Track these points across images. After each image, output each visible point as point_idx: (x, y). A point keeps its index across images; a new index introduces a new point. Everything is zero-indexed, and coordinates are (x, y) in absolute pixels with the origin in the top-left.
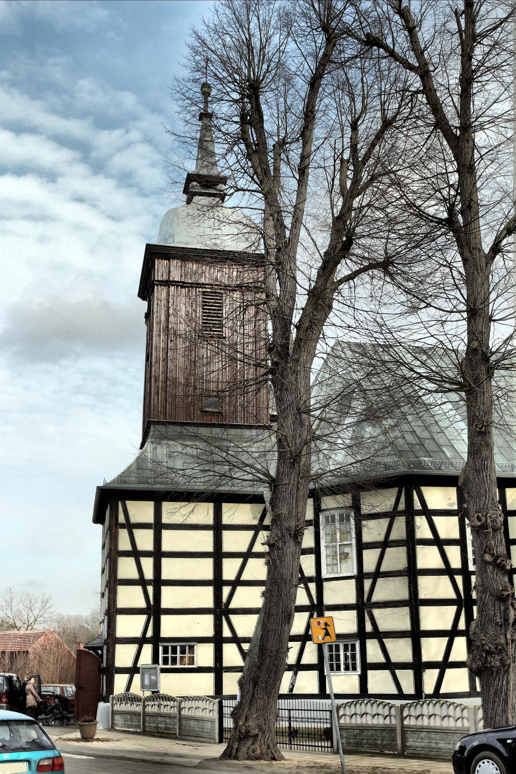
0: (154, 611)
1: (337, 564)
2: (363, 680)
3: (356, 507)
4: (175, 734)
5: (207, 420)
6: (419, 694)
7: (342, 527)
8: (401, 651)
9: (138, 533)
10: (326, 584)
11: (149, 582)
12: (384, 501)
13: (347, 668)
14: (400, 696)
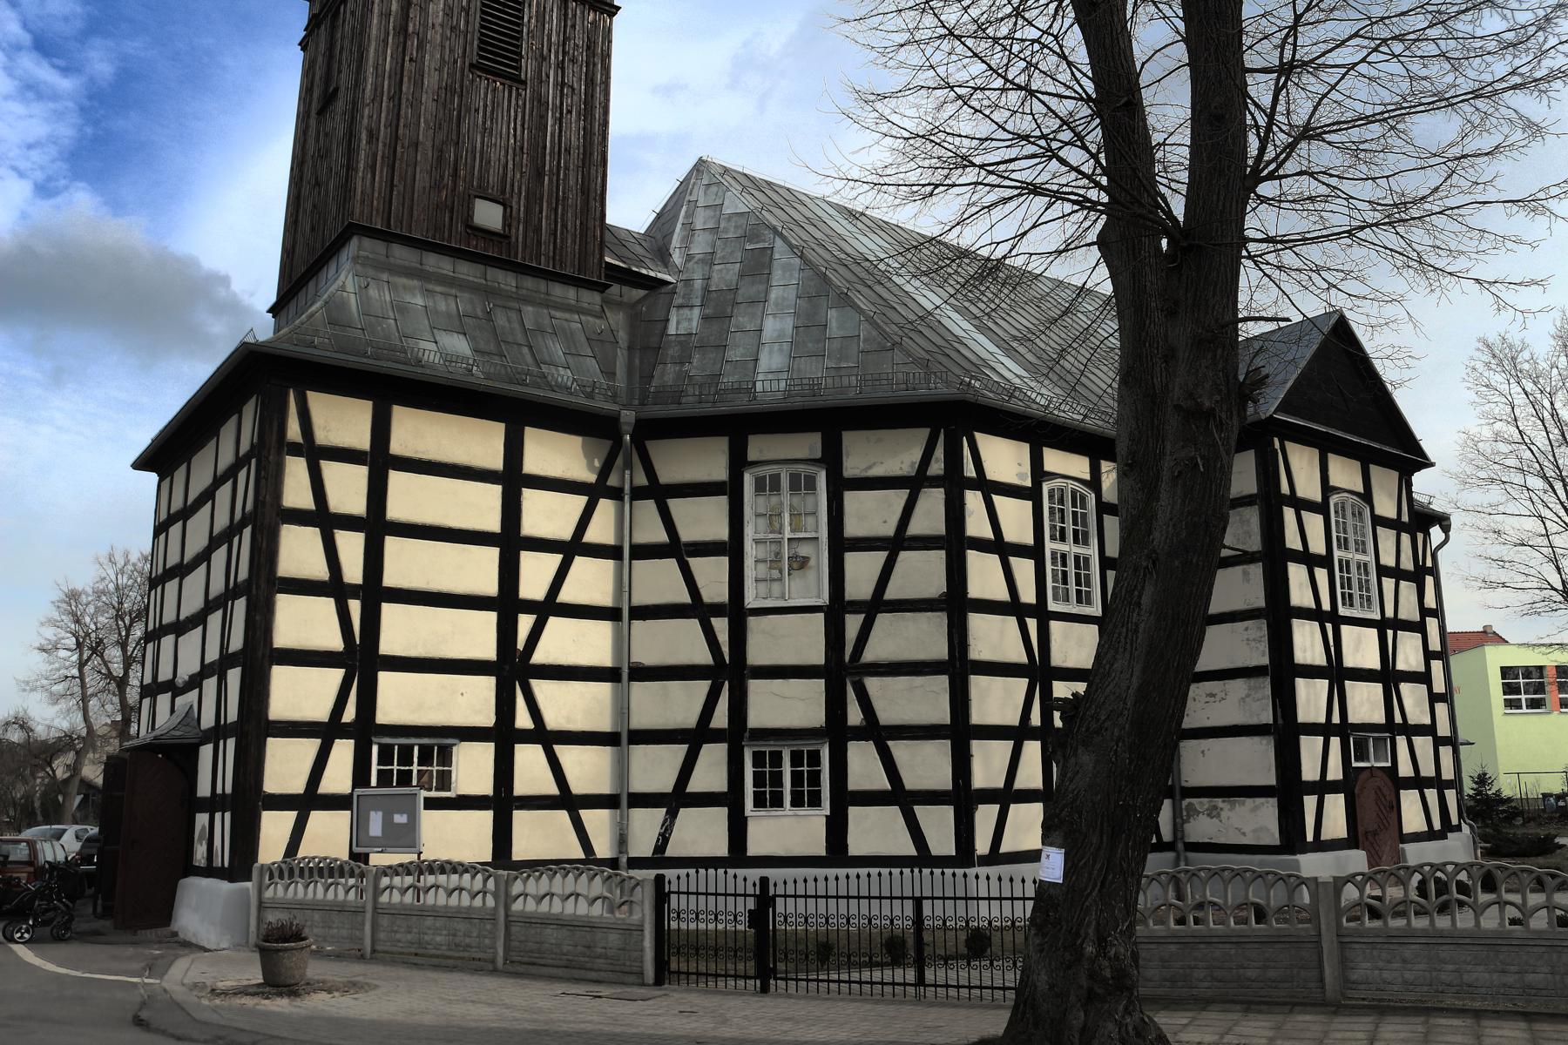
0: (362, 660)
1: (780, 580)
2: (837, 829)
3: (832, 459)
4: (493, 961)
5: (476, 246)
6: (965, 853)
7: (796, 500)
8: (926, 765)
9: (332, 471)
10: (753, 622)
11: (354, 591)
12: (899, 453)
13: (797, 802)
14: (924, 858)
